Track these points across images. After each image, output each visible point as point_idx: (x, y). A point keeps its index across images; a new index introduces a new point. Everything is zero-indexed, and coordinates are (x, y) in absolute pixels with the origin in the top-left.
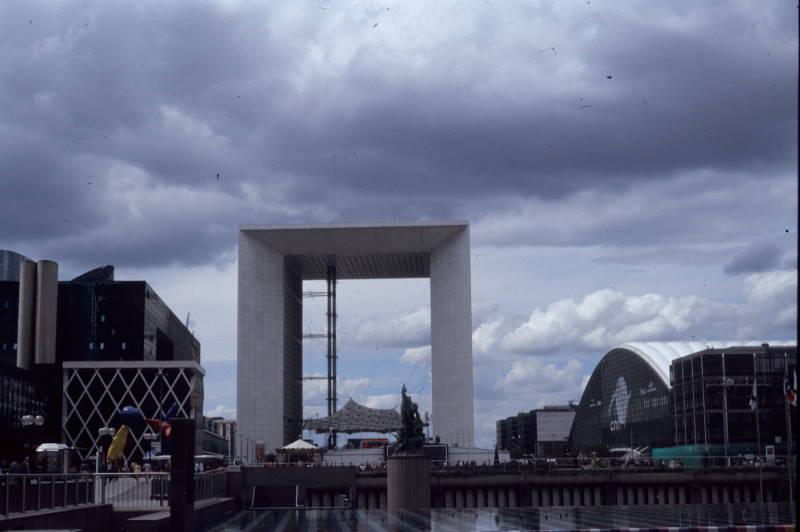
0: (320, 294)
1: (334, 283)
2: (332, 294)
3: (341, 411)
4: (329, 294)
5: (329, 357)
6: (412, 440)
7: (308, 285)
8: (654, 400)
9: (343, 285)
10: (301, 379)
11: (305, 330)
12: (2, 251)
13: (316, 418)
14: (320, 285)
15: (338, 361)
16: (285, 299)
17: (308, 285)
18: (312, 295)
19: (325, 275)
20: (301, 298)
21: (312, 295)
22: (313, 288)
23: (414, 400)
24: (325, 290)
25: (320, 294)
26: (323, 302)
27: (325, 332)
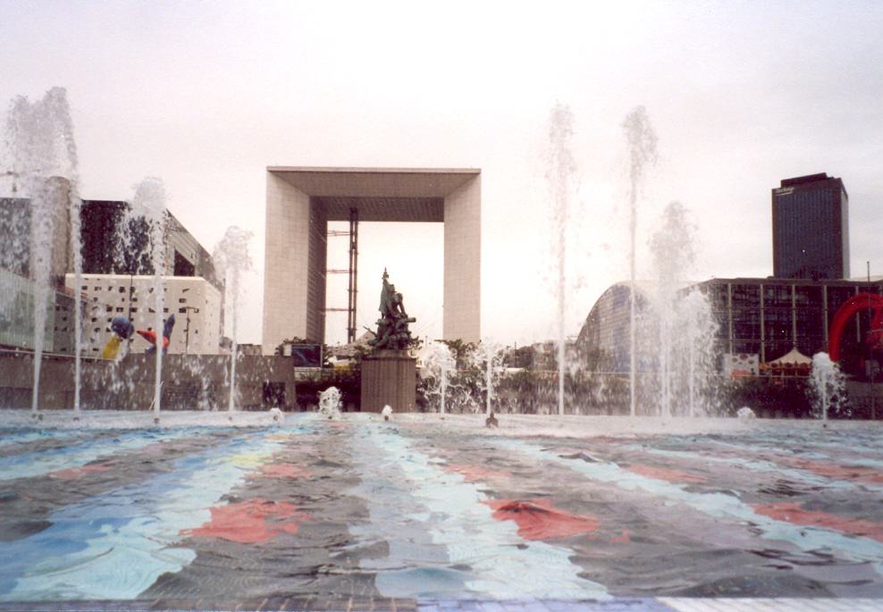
0: (343, 234)
1: (356, 224)
2: (354, 234)
3: (360, 340)
4: (350, 310)
5: (350, 291)
6: (394, 337)
7: (332, 225)
8: (362, 593)
9: (364, 226)
10: (324, 271)
11: (328, 305)
12: (878, 417)
13: (337, 345)
14: (345, 226)
15: (358, 294)
16: (310, 237)
17: (332, 225)
18: (335, 233)
19: (348, 216)
20: (325, 237)
21: (335, 233)
22: (338, 229)
23: (398, 290)
24: (348, 230)
25: (343, 234)
26: (345, 242)
27: (347, 307)
